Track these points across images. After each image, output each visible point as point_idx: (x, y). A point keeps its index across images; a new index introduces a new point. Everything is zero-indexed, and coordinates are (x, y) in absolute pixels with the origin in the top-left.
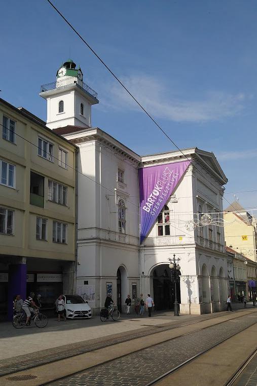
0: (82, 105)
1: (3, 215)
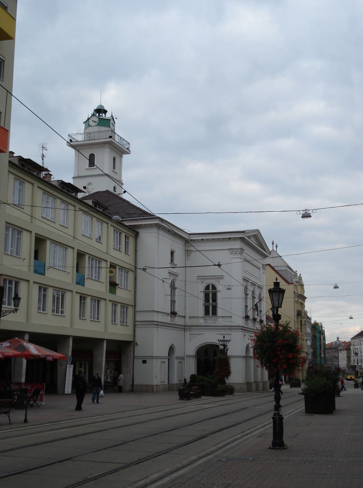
0: (114, 159)
1: (358, 387)
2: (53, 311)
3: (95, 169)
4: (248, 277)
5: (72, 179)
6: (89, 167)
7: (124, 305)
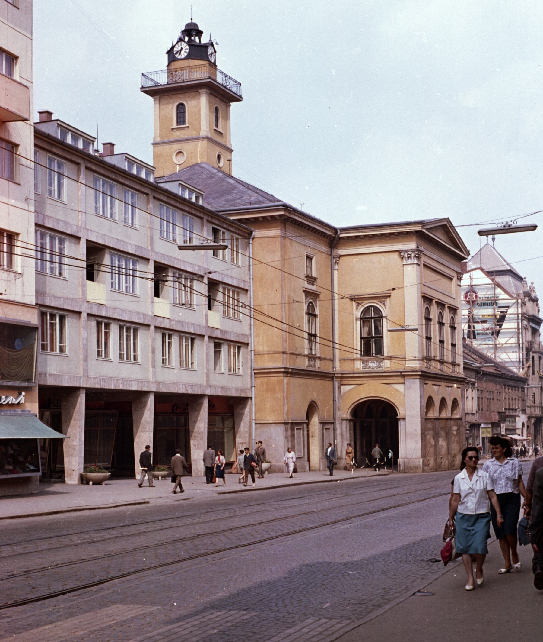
0: (217, 109)
2: (99, 354)
3: (186, 129)
4: (431, 293)
5: (152, 146)
6: (177, 125)
7: (54, 311)
